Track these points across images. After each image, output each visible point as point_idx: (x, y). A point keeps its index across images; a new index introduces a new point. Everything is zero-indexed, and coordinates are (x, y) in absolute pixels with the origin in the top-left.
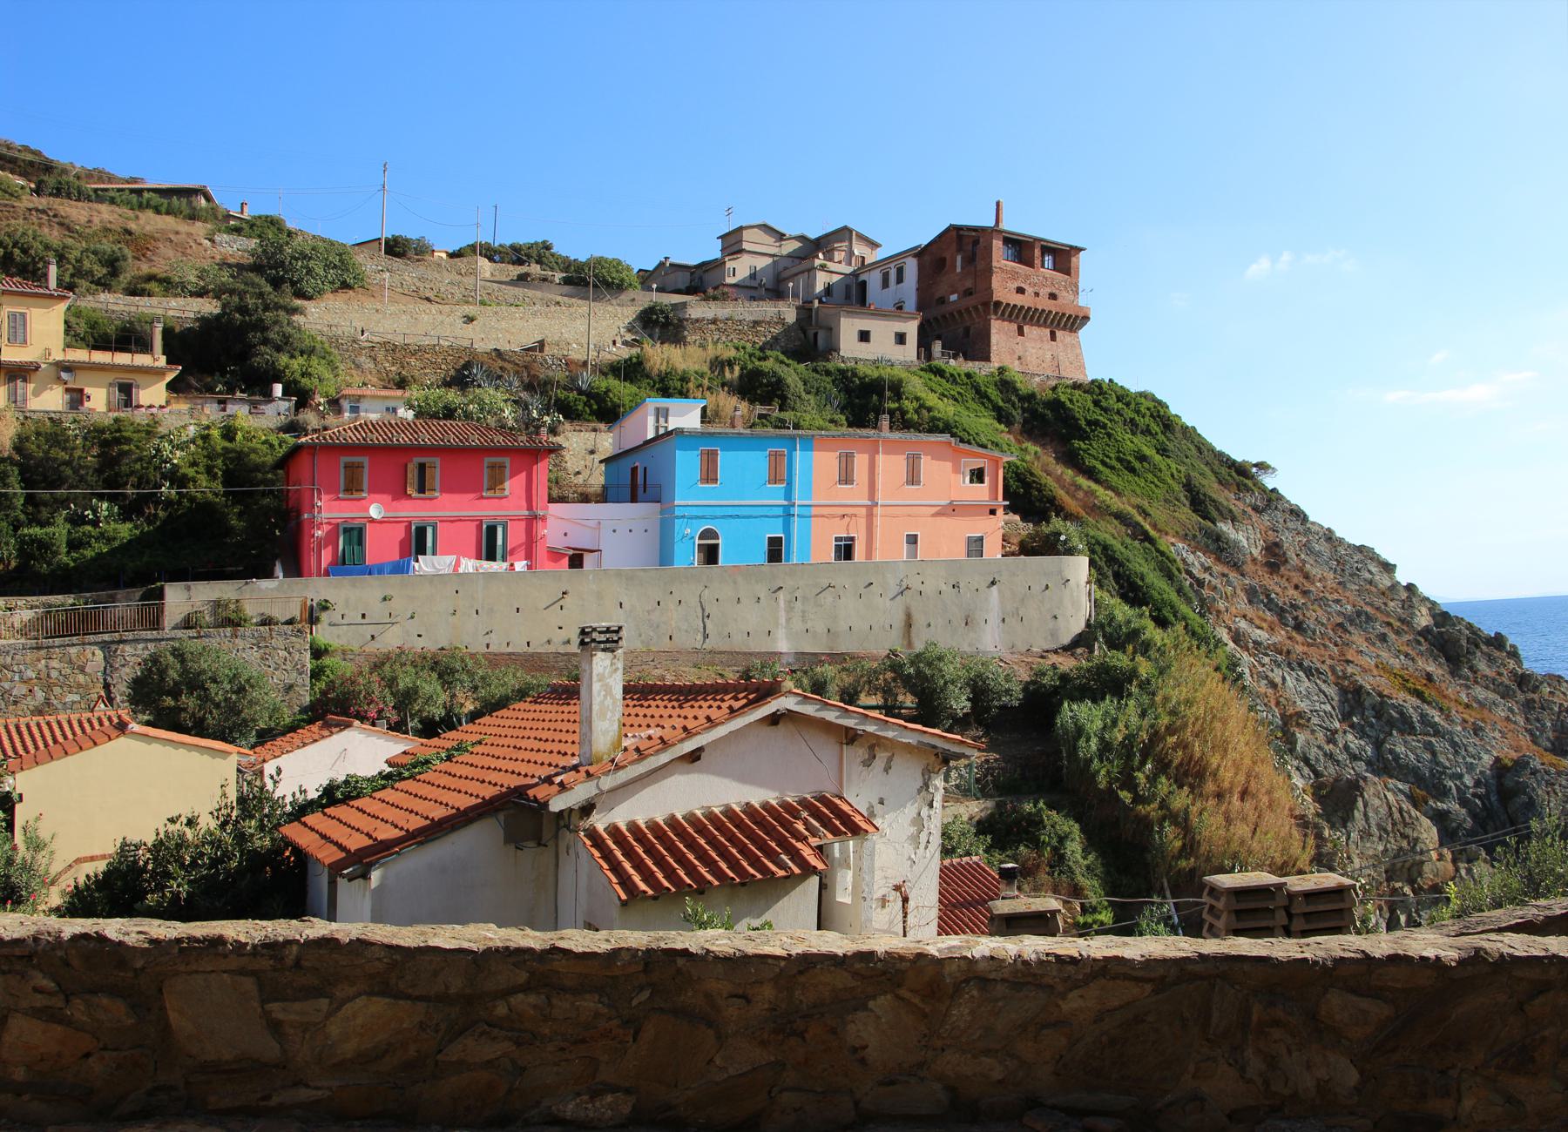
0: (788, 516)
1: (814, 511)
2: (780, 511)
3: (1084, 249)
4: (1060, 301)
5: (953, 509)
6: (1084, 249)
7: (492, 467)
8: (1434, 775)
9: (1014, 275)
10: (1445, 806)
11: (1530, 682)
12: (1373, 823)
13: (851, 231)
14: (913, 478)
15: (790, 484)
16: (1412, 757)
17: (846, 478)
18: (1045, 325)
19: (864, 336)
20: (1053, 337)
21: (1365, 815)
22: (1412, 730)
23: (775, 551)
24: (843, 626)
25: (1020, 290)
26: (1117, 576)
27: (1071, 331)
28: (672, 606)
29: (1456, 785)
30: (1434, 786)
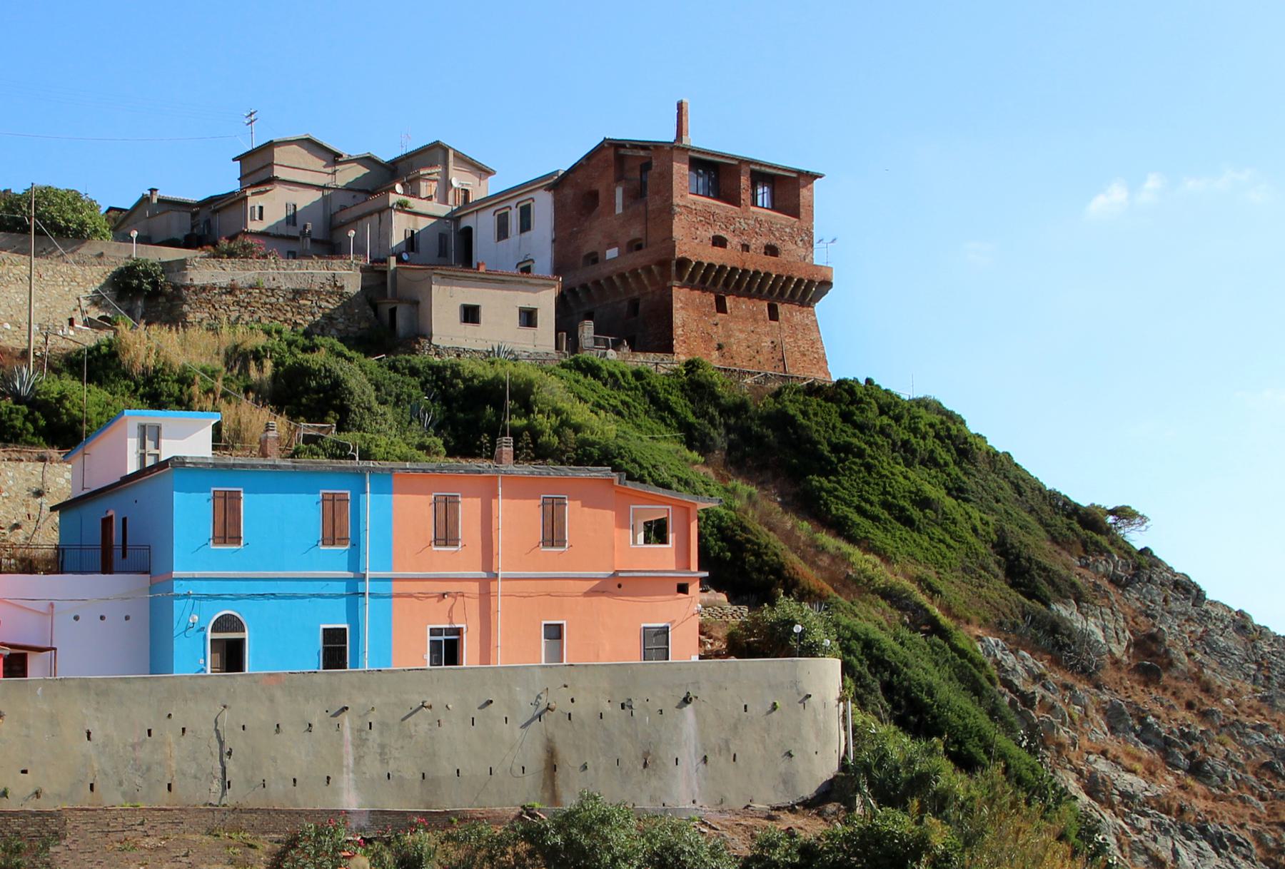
0: (354, 595)
1: (396, 587)
3: (821, 177)
4: (783, 257)
13: (445, 150)
14: (553, 535)
15: (356, 546)
17: (446, 535)
18: (759, 295)
20: (774, 315)
24: (445, 769)
25: (719, 242)
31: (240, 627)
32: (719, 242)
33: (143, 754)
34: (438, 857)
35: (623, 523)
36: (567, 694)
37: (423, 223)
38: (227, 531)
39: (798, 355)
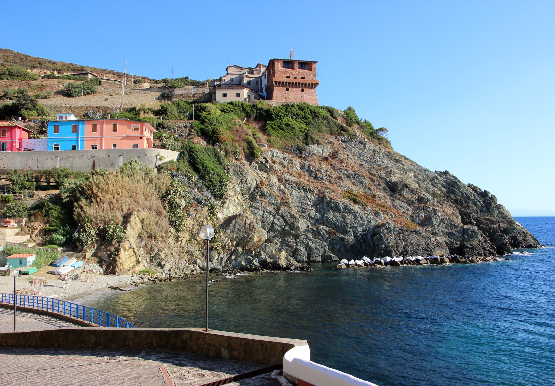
0: (77, 140)
1: (85, 139)
2: (75, 139)
3: (317, 62)
4: (306, 79)
5: (128, 138)
6: (317, 62)
7: (3, 131)
8: (342, 226)
9: (285, 72)
10: (344, 236)
11: (423, 200)
12: (236, 228)
13: (260, 65)
14: (115, 130)
15: (78, 132)
16: (334, 219)
17: (94, 130)
18: (299, 87)
19: (225, 95)
20: (303, 91)
21: (235, 226)
22: (339, 211)
23: (74, 148)
24: (75, 165)
25: (288, 77)
26: (190, 155)
27: (312, 88)
28: (30, 160)
29: (353, 230)
30: (343, 230)
31: (58, 145)
32: (288, 77)
33: (26, 162)
34: (333, 180)
35: (129, 128)
36: (98, 154)
37: (252, 79)
38: (56, 131)
39: (309, 99)
